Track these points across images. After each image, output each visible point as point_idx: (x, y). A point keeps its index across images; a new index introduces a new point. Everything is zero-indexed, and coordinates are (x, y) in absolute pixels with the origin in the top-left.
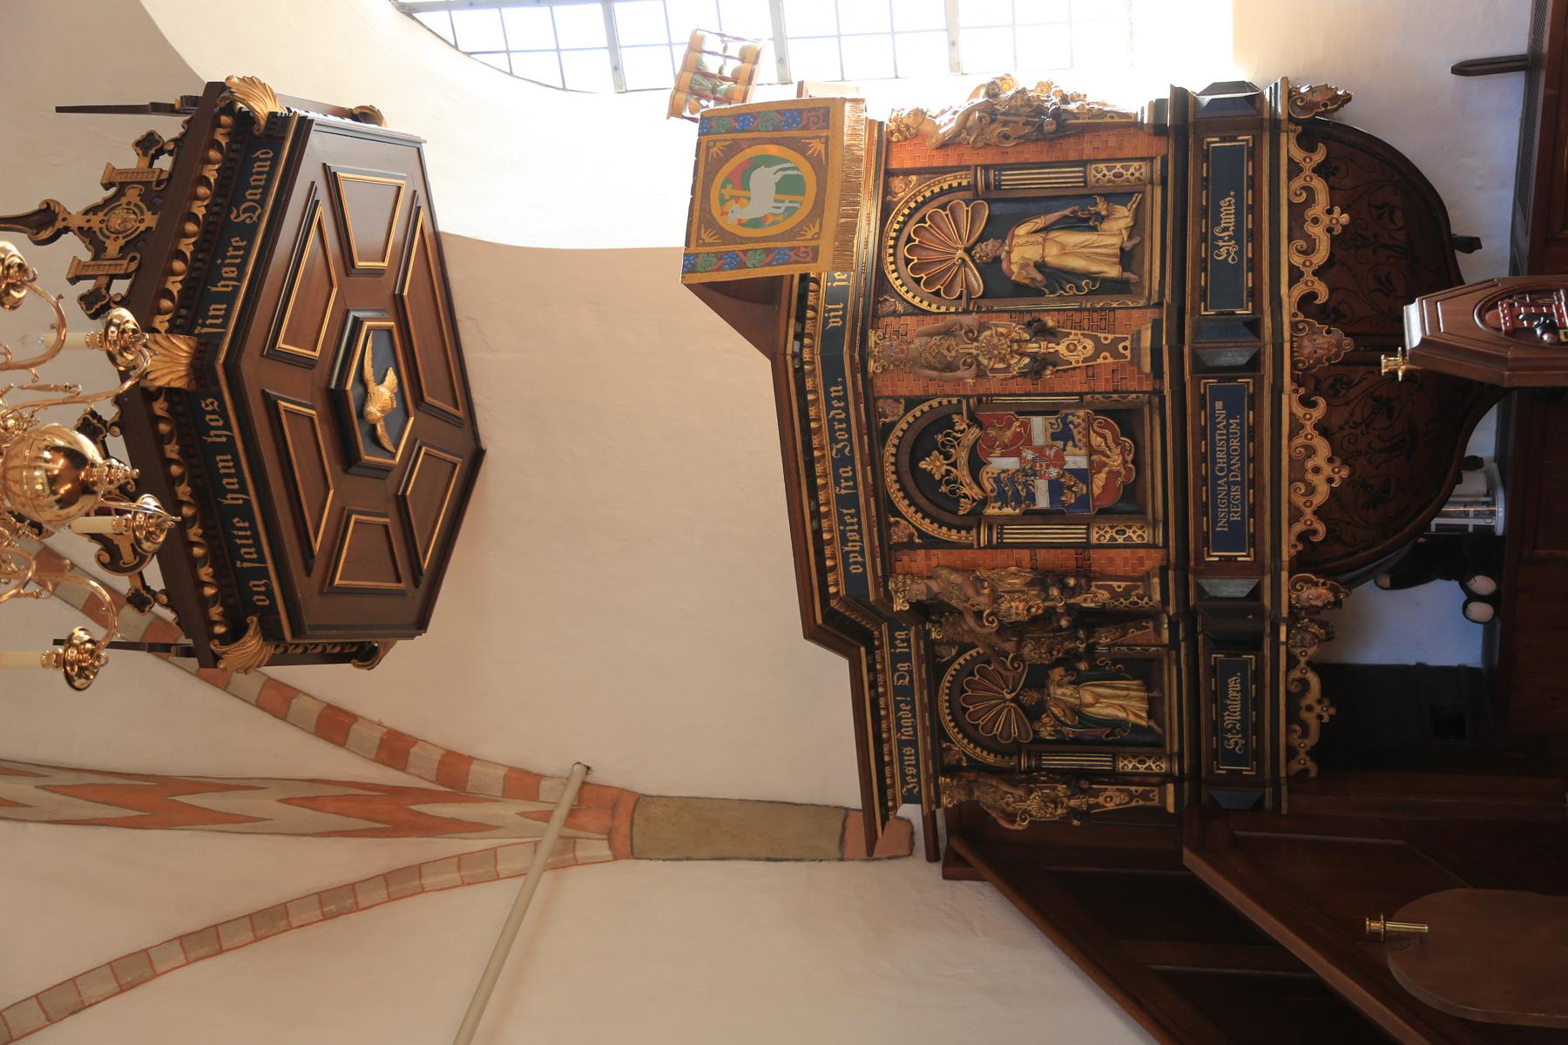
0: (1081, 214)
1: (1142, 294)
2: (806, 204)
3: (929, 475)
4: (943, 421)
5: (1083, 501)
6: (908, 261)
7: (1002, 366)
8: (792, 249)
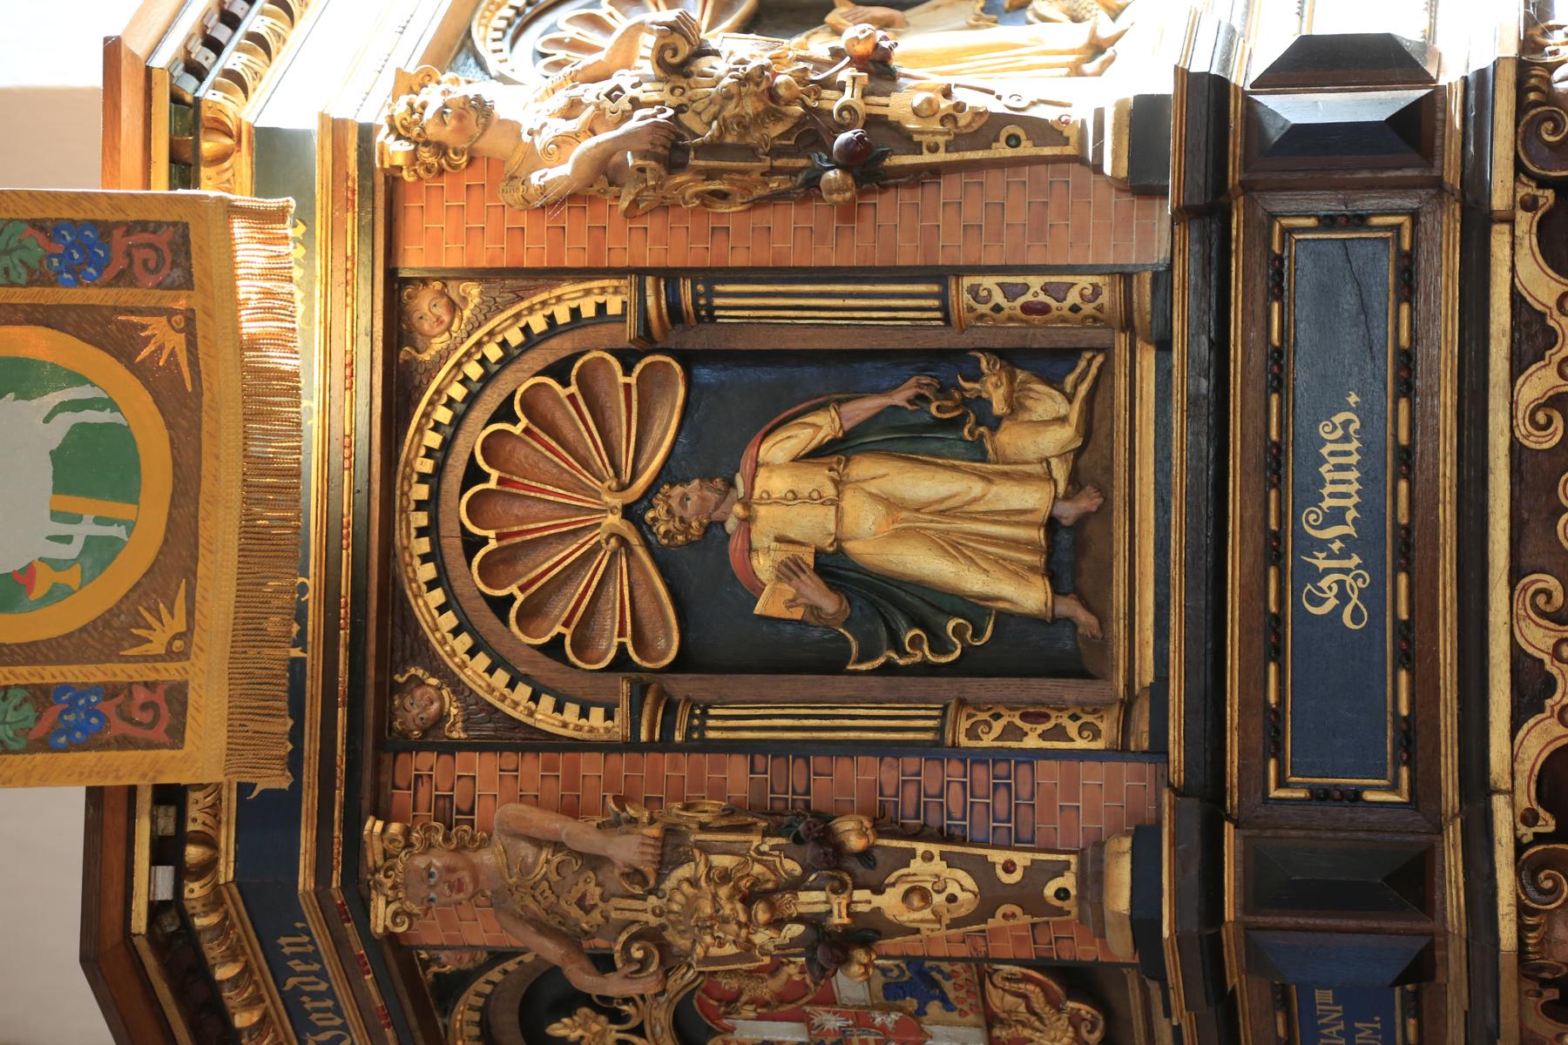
0: (929, 394)
2: (145, 525)
8: (110, 691)
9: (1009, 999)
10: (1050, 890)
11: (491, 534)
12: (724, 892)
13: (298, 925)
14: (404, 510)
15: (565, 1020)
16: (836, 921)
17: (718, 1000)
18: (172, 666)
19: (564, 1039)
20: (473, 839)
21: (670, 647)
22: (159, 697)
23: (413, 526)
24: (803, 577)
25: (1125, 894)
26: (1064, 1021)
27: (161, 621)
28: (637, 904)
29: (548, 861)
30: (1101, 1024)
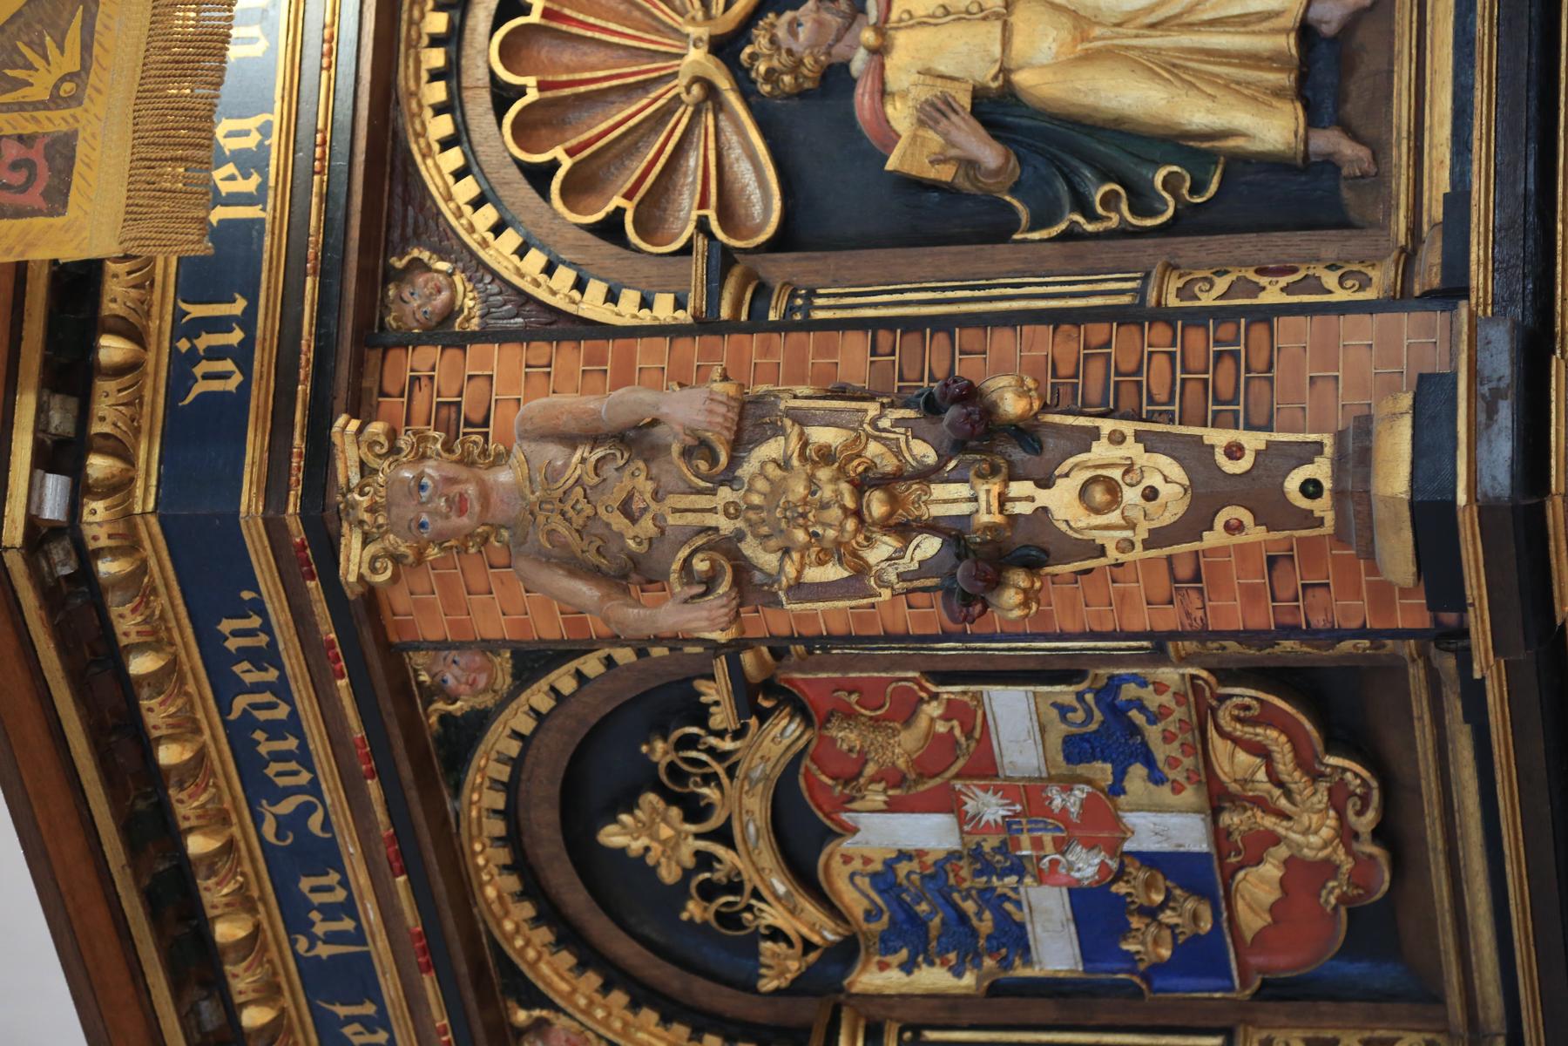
1: (1384, 227)
3: (638, 868)
4: (674, 704)
5: (1200, 956)
6: (503, 96)
7: (833, 572)
9: (1242, 757)
10: (1293, 483)
11: (530, 81)
12: (824, 474)
13: (247, 595)
14: (413, 45)
15: (625, 818)
16: (984, 518)
17: (832, 778)
18: (56, 115)
19: (622, 851)
20: (484, 453)
21: (765, 206)
22: (37, 154)
23: (424, 67)
24: (954, 117)
25: (1404, 470)
26: (1322, 797)
27: (45, 57)
28: (702, 501)
29: (583, 460)
30: (1376, 795)
